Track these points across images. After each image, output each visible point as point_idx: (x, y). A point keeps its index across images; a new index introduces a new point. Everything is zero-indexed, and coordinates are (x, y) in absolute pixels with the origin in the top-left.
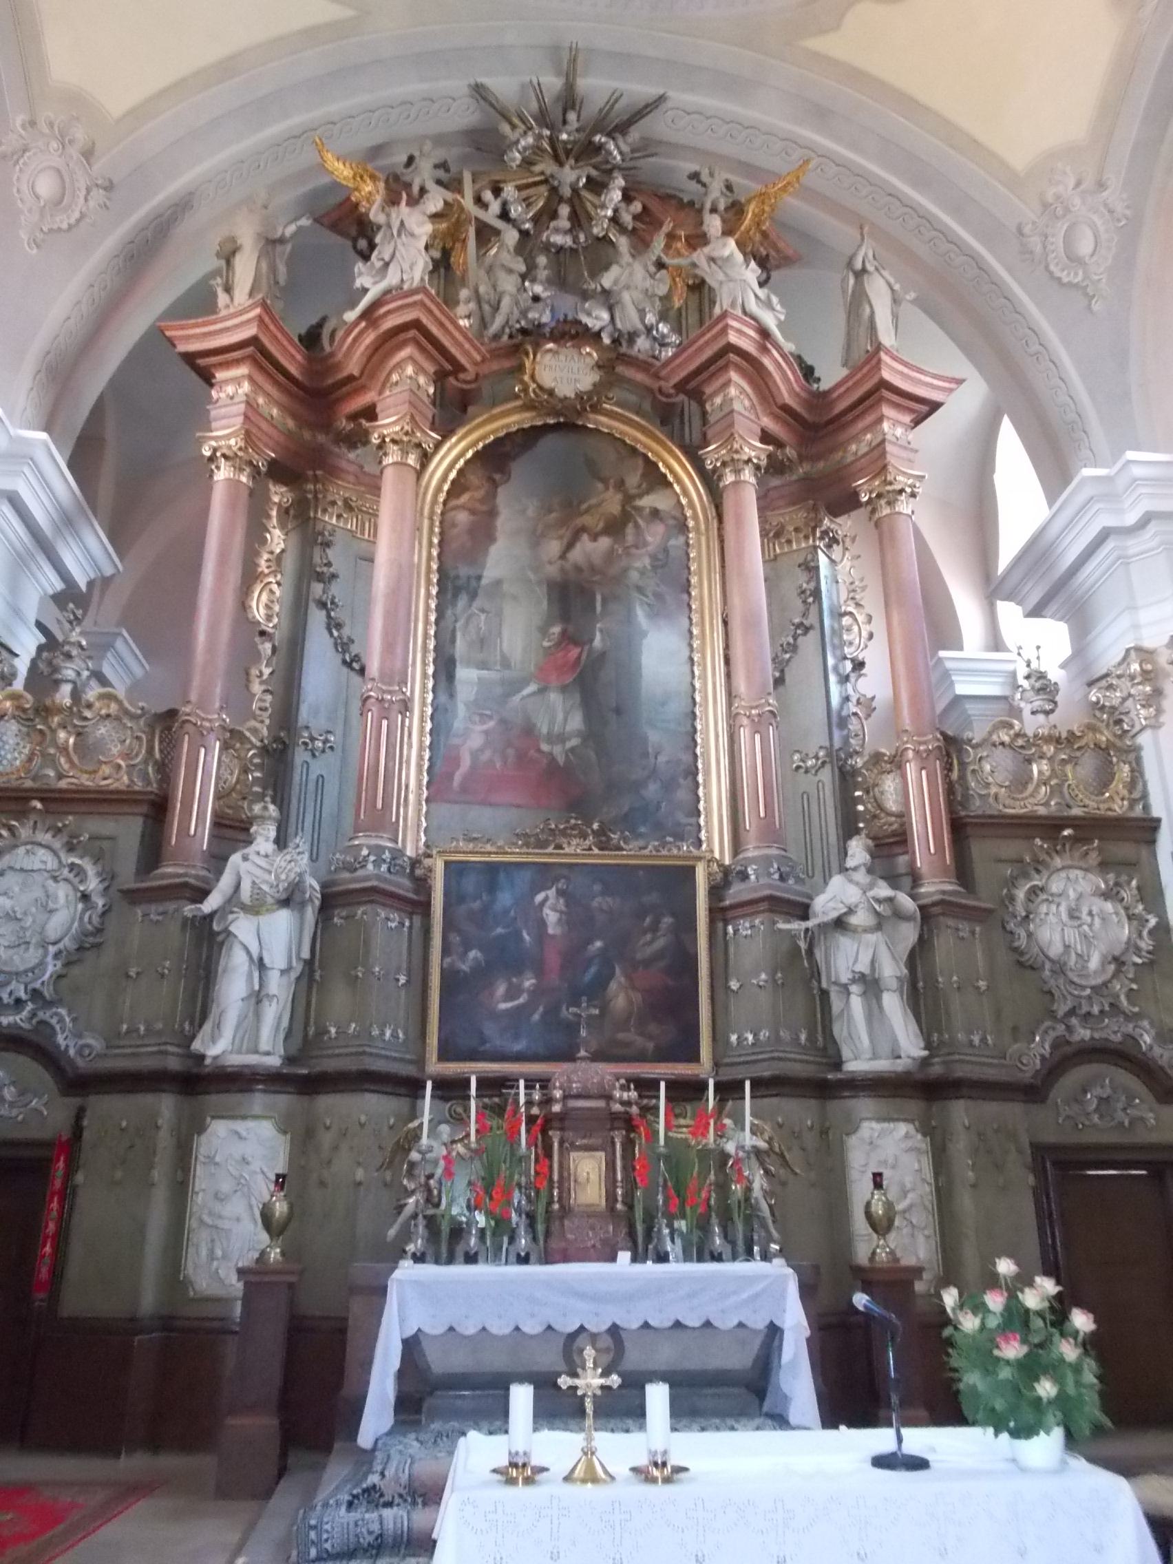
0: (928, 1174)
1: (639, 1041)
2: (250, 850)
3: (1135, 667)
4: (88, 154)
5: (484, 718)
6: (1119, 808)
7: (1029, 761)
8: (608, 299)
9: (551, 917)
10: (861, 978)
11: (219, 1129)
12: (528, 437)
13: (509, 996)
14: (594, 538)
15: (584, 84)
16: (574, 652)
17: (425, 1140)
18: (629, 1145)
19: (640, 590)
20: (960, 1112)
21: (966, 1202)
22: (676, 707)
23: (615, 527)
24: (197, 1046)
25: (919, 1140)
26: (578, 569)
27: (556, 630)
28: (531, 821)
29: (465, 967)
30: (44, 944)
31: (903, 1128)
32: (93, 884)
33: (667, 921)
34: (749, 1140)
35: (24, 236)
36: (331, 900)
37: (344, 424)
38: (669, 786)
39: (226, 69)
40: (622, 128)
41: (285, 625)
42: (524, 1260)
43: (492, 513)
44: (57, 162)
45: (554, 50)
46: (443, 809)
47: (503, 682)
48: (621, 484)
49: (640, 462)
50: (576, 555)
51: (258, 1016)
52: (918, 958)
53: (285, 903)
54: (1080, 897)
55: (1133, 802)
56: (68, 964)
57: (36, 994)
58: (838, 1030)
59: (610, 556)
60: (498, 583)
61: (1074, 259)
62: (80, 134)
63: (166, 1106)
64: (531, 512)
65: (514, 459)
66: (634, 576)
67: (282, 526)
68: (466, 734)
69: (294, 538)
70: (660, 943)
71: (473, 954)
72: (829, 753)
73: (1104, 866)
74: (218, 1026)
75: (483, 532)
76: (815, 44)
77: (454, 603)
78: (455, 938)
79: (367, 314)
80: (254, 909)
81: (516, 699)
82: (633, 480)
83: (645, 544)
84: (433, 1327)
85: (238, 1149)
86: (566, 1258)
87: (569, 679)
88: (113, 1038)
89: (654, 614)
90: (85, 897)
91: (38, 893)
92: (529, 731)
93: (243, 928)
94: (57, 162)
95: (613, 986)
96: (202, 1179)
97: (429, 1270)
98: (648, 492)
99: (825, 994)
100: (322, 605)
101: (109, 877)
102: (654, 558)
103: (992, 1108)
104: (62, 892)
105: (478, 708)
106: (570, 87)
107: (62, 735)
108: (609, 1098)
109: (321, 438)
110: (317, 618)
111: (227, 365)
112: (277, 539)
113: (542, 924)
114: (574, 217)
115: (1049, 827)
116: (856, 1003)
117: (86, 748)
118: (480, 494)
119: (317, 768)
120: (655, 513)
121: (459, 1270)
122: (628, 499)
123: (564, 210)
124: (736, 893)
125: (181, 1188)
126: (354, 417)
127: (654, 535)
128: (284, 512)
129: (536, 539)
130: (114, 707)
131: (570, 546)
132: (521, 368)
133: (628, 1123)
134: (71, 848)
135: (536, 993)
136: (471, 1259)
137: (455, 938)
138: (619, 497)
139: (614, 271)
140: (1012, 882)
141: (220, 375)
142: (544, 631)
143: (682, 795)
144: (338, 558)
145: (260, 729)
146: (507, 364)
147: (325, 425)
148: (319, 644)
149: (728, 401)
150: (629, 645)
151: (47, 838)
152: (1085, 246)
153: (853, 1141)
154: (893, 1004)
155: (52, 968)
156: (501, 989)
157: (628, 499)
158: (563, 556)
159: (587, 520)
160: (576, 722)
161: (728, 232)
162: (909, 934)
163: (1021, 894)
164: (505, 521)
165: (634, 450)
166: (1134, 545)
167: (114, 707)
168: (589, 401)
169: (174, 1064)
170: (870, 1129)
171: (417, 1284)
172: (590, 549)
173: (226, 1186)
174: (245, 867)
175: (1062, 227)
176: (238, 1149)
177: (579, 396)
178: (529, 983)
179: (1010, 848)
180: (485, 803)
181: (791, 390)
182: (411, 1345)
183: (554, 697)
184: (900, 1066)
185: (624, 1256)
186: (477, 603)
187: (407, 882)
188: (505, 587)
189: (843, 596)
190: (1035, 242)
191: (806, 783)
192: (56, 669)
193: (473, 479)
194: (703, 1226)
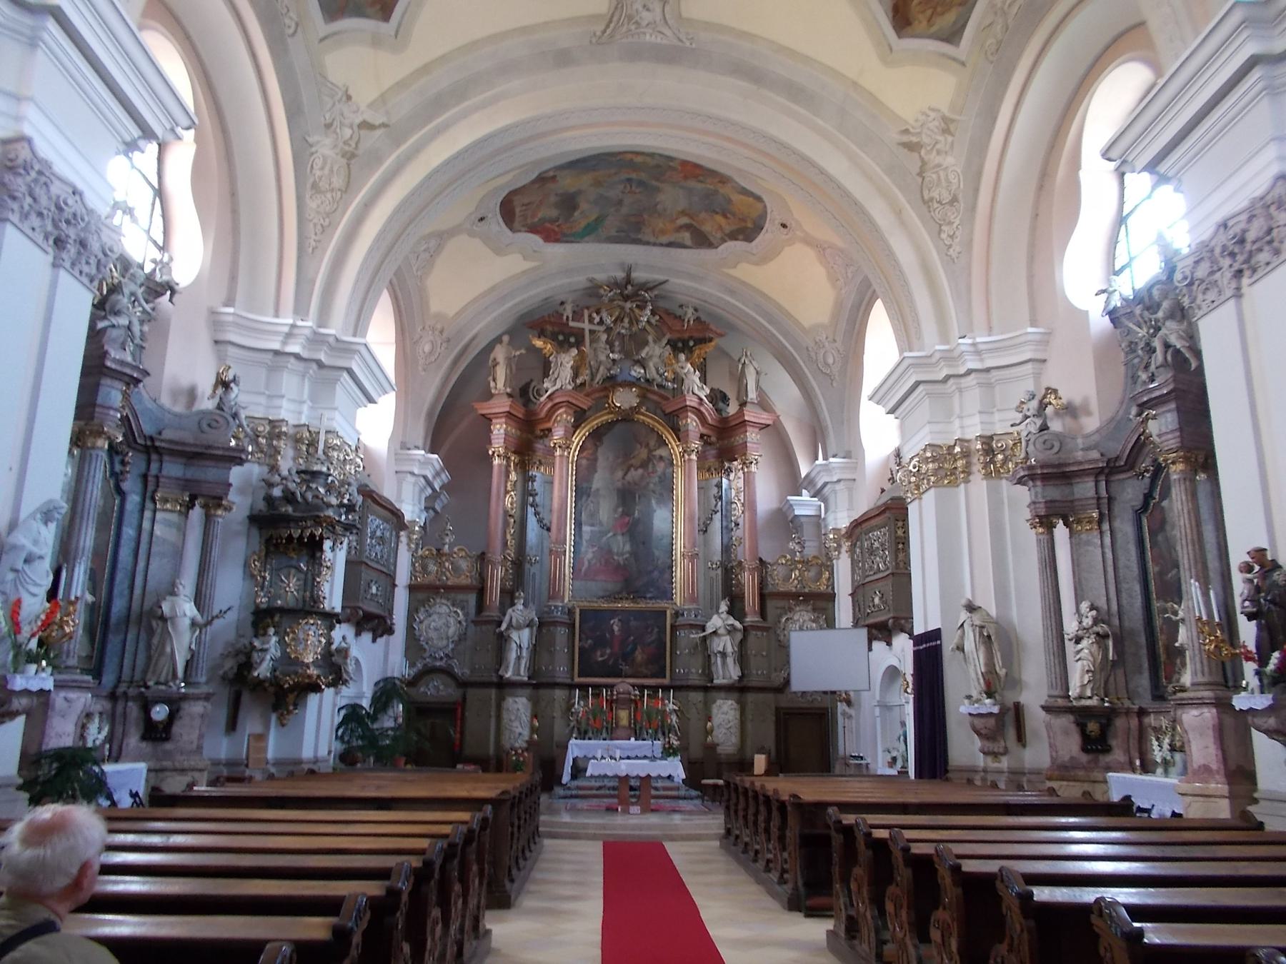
0: (738, 717)
1: (645, 671)
2: (515, 608)
3: (929, 454)
4: (441, 332)
5: (593, 546)
6: (823, 588)
7: (792, 571)
8: (642, 363)
9: (616, 628)
10: (720, 652)
11: (510, 700)
12: (608, 426)
13: (602, 656)
14: (636, 469)
15: (634, 275)
16: (627, 519)
17: (576, 706)
18: (636, 707)
19: (654, 492)
20: (751, 697)
21: (749, 726)
22: (666, 541)
23: (644, 465)
24: (500, 673)
25: (735, 705)
26: (629, 483)
27: (620, 510)
28: (611, 587)
29: (586, 646)
30: (448, 638)
31: (730, 702)
32: (461, 617)
33: (656, 630)
34: (671, 706)
35: (420, 368)
36: (541, 625)
37: (538, 432)
38: (662, 572)
39: (493, 289)
40: (651, 289)
41: (518, 512)
42: (604, 739)
43: (596, 460)
44: (432, 338)
45: (622, 265)
46: (577, 583)
47: (600, 532)
48: (647, 445)
49: (655, 436)
50: (629, 477)
51: (519, 665)
52: (742, 643)
53: (528, 626)
54: (804, 621)
55: (828, 587)
56: (456, 645)
57: (447, 655)
58: (713, 669)
59: (642, 477)
60: (598, 490)
61: (826, 364)
62: (439, 326)
63: (493, 693)
64: (611, 459)
65: (605, 434)
66: (652, 486)
67: (515, 470)
68: (586, 552)
69: (520, 477)
70: (653, 638)
71: (590, 641)
72: (721, 563)
73: (814, 610)
74: (508, 667)
75: (592, 468)
76: (726, 270)
77: (581, 499)
78: (583, 636)
79: (549, 397)
80: (519, 628)
81: (605, 539)
82: (652, 443)
83: (656, 471)
84: (581, 755)
85: (516, 706)
86: (617, 739)
87: (625, 530)
88: (473, 670)
89: (659, 502)
90: (460, 622)
91: (444, 621)
92: (610, 551)
93: (514, 635)
94: (432, 338)
95: (637, 653)
96: (505, 715)
97: (579, 742)
98: (659, 448)
99: (709, 656)
100: (532, 506)
101: (466, 615)
102: (660, 477)
103: (761, 696)
104: (452, 620)
105: (591, 543)
106: (629, 275)
107: (447, 564)
108: (630, 694)
109: (530, 436)
110: (531, 510)
111: (497, 418)
112: (513, 476)
113: (613, 631)
114: (631, 323)
115: (795, 596)
116: (719, 660)
117: (456, 569)
118: (590, 452)
119: (533, 570)
120: (661, 458)
121: (586, 742)
122: (650, 451)
123: (626, 320)
124: (681, 620)
125: (499, 717)
126: (542, 430)
127: (660, 467)
128: (516, 465)
129: (612, 470)
130: (464, 554)
131: (626, 474)
132: (607, 397)
133: (635, 702)
134: (453, 605)
135: (611, 655)
136: (590, 739)
137: (583, 636)
138: (646, 451)
139: (647, 349)
140: (780, 616)
141: (494, 421)
142: (615, 511)
143: (667, 576)
144: (537, 485)
145: (511, 553)
146: (602, 394)
147: (532, 431)
148: (532, 522)
149: (687, 424)
150: (649, 515)
151: (443, 601)
152: (830, 361)
153: (714, 706)
154: (730, 660)
155: (451, 646)
156: (599, 653)
157: (650, 451)
158: (623, 478)
159: (633, 462)
160: (628, 548)
161: (687, 359)
162: (739, 636)
163: (784, 620)
164: (601, 463)
165: (653, 430)
166: (838, 487)
167: (464, 554)
168: (634, 410)
169: (495, 679)
170: (719, 702)
171: (576, 745)
172: (635, 474)
173: (513, 718)
174: (513, 614)
175: (822, 351)
176: (516, 706)
177: (631, 408)
178: (608, 651)
179: (781, 603)
180: (593, 580)
181: (712, 419)
182: (574, 760)
183: (620, 538)
184: (731, 682)
185: (633, 739)
186: (591, 499)
187: (566, 617)
188: (601, 492)
189: (733, 494)
190: (813, 354)
191: (713, 573)
192: (443, 539)
193: (589, 445)
194: (656, 732)
